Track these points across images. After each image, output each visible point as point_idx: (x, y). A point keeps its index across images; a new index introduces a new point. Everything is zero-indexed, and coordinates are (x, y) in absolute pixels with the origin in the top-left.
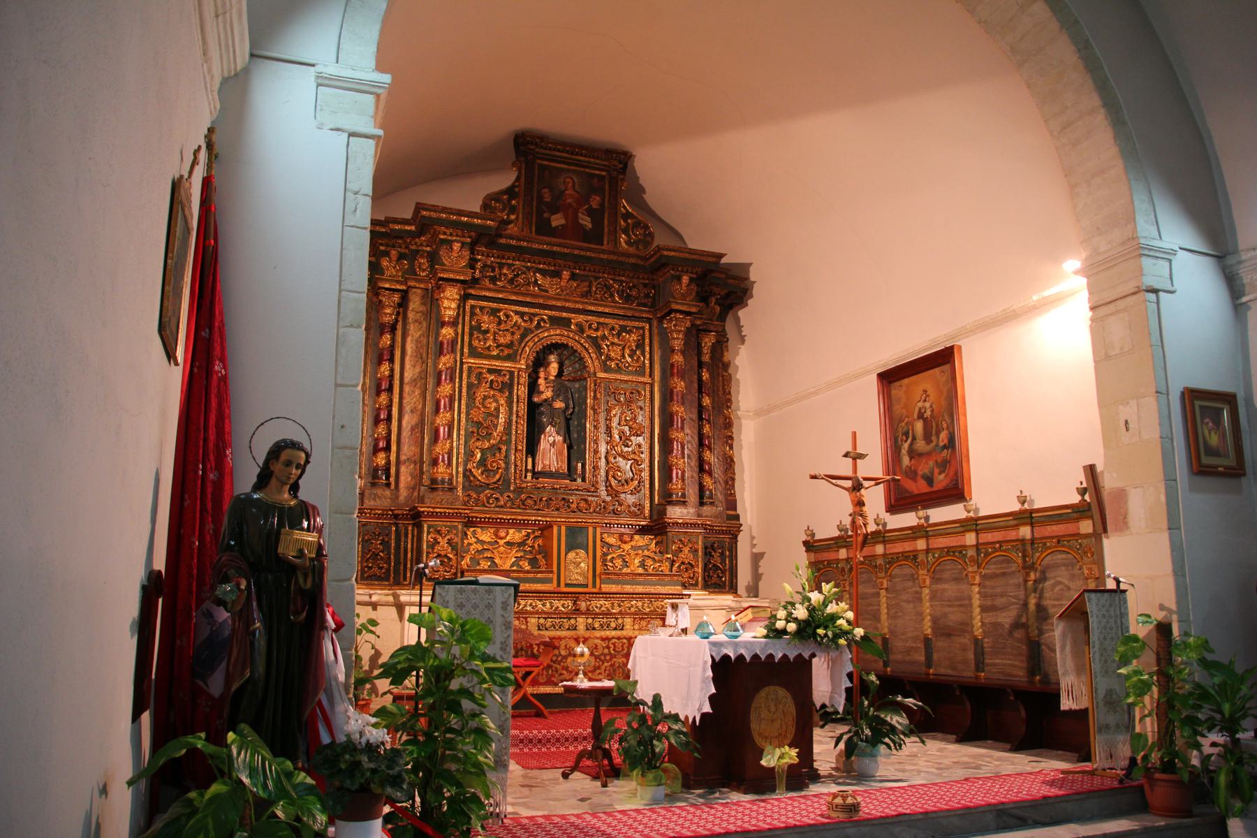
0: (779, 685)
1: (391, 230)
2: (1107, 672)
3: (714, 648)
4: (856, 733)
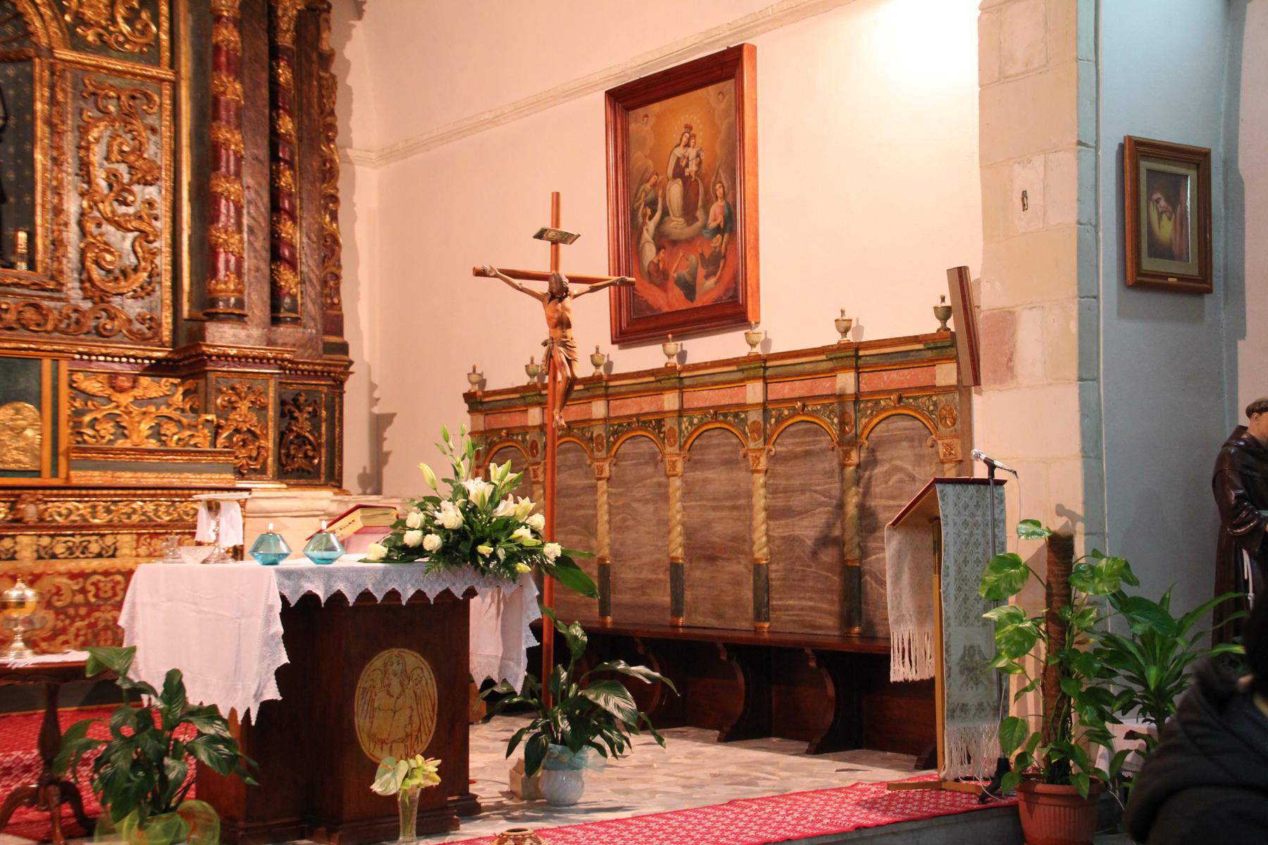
0: (409, 647)
2: (966, 617)
3: (286, 582)
4: (547, 729)
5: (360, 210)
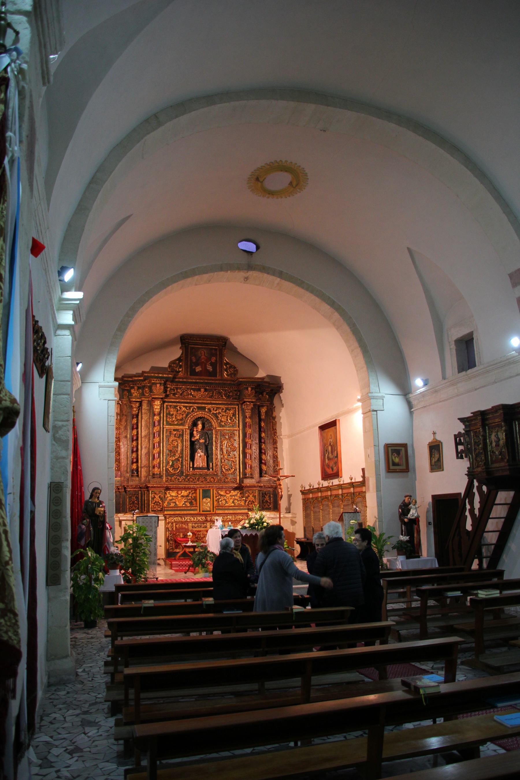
5: (284, 449)
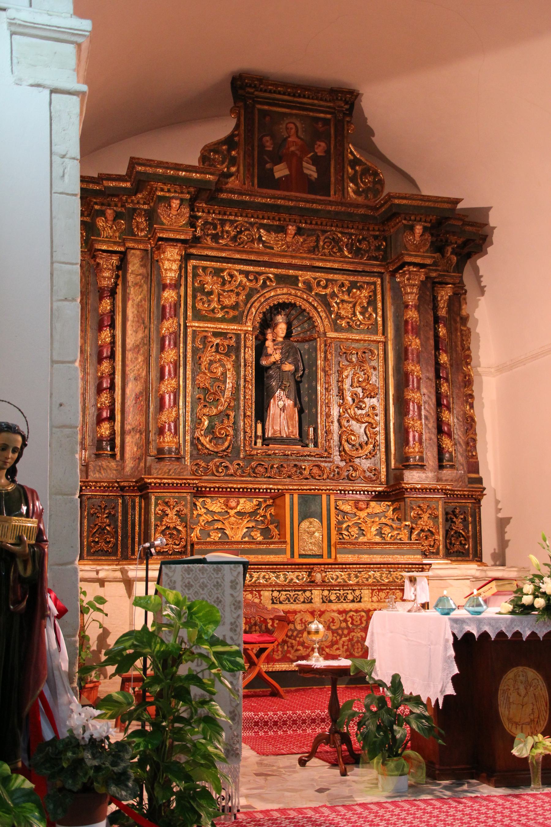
0: (529, 666)
1: (105, 187)
3: (455, 625)
